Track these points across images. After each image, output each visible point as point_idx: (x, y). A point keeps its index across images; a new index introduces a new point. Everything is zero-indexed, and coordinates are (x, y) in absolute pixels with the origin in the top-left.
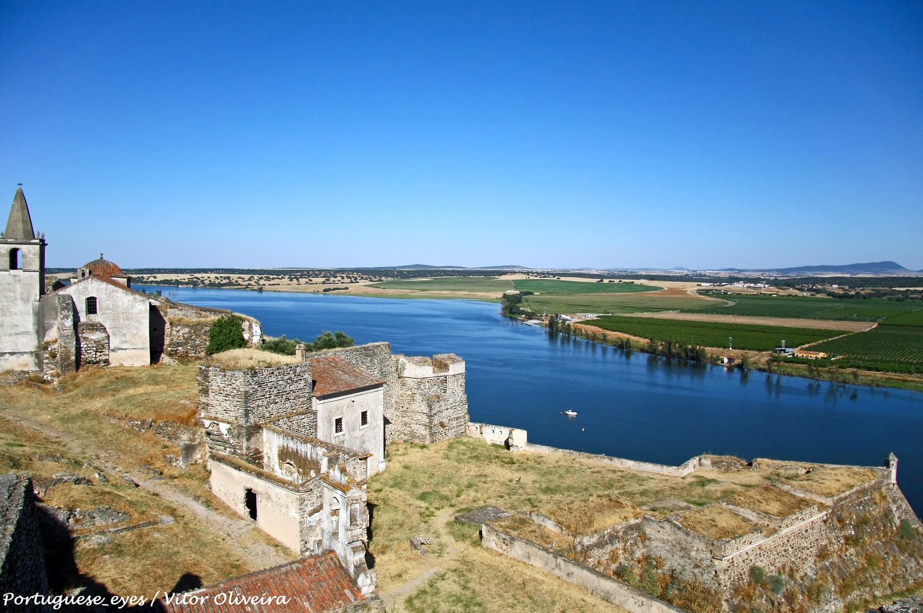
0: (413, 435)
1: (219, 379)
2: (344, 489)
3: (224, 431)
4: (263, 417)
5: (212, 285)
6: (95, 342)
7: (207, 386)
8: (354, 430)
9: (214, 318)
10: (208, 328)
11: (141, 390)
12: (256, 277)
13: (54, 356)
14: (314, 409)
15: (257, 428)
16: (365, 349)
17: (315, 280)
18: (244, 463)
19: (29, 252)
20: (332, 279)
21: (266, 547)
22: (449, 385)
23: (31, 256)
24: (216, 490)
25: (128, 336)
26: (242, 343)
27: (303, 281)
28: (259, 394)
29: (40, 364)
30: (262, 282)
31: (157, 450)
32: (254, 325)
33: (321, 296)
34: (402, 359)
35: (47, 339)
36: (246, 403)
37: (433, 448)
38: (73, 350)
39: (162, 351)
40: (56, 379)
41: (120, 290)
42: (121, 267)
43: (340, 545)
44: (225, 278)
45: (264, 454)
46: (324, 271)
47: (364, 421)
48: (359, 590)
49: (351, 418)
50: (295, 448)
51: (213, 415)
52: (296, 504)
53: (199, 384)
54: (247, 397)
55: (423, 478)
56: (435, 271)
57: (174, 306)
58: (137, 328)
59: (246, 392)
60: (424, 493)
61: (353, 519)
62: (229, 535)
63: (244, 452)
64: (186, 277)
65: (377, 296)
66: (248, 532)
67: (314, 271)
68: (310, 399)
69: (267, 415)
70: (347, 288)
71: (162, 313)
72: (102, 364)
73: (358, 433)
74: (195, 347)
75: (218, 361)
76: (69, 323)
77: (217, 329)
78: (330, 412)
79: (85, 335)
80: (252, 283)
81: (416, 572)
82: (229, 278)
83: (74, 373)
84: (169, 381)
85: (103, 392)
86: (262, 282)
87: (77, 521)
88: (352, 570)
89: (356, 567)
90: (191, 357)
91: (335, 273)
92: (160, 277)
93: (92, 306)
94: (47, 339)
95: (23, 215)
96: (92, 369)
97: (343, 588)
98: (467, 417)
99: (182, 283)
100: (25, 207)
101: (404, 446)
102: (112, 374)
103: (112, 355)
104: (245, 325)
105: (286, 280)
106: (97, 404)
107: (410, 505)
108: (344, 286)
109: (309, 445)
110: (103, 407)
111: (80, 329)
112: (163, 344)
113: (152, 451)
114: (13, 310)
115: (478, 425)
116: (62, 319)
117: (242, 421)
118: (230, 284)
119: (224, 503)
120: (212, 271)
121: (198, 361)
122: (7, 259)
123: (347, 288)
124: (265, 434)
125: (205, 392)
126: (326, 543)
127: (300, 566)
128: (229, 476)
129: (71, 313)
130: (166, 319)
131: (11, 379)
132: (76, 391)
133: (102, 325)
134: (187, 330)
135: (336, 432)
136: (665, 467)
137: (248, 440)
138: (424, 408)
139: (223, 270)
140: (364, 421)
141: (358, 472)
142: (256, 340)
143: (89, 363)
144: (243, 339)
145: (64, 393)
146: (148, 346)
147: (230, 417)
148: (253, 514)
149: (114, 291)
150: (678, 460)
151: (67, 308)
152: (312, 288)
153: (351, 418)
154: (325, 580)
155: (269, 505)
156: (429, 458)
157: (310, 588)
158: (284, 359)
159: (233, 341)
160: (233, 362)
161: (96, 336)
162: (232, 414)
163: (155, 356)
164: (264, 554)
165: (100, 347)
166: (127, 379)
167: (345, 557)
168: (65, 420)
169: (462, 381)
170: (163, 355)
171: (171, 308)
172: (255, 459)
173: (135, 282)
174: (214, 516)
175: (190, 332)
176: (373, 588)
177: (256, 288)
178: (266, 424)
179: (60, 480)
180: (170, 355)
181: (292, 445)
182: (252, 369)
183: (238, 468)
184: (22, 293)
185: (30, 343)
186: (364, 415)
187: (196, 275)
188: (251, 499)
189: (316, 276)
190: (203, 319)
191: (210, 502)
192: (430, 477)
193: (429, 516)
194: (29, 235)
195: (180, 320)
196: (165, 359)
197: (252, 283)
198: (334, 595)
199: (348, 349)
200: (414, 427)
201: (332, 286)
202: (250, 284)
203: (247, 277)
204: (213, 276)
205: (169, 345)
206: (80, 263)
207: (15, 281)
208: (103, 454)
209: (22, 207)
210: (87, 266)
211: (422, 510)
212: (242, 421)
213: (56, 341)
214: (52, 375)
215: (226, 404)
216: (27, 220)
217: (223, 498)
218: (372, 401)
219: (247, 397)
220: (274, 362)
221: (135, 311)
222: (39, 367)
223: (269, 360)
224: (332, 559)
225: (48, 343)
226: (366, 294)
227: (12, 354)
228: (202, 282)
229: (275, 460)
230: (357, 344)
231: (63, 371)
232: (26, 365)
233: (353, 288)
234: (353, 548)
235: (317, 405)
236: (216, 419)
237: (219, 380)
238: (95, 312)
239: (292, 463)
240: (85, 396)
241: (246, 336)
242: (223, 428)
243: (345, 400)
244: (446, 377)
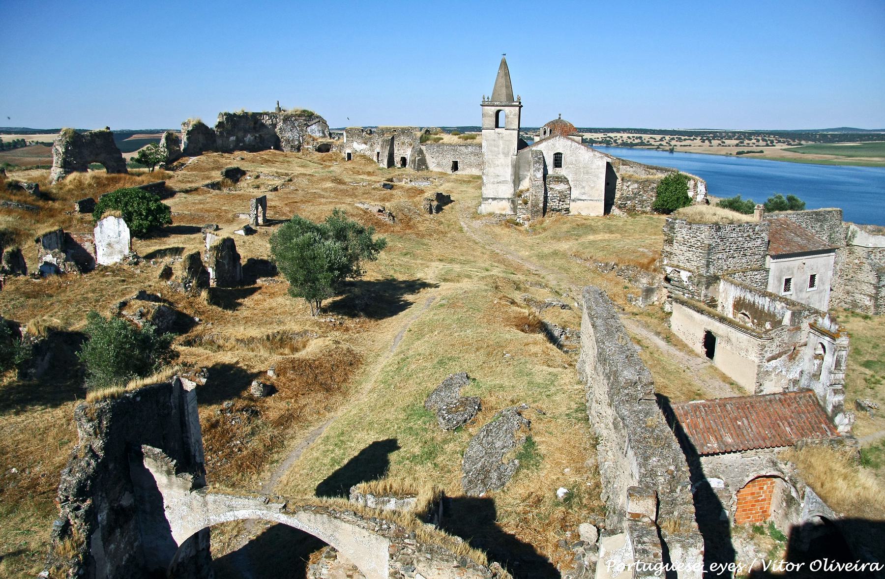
0: (855, 304)
1: (684, 231)
2: (833, 337)
3: (685, 279)
4: (722, 269)
5: (625, 145)
7: (672, 237)
8: (801, 291)
9: (661, 176)
10: (655, 185)
11: (599, 237)
12: (667, 138)
13: (526, 203)
14: (767, 266)
15: (716, 279)
16: (817, 214)
17: (728, 142)
18: (706, 307)
20: (746, 141)
21: (722, 384)
27: (715, 142)
28: (720, 248)
29: (514, 209)
30: (673, 143)
31: (618, 290)
32: (699, 184)
33: (734, 159)
34: (853, 227)
35: (521, 188)
36: (709, 254)
37: (877, 319)
38: (542, 199)
39: (613, 204)
40: (526, 222)
43: (821, 386)
44: (637, 138)
45: (719, 303)
46: (738, 132)
48: (836, 427)
49: (799, 279)
50: (752, 300)
51: (676, 263)
52: (757, 349)
53: (665, 235)
54: (710, 249)
55: (867, 347)
56: (865, 135)
57: (625, 163)
58: (594, 182)
59: (710, 245)
60: (868, 362)
61: (838, 364)
62: (688, 368)
63: (702, 298)
64: (600, 136)
65: (795, 161)
66: (705, 368)
67: (727, 133)
68: (764, 257)
69: (725, 267)
70: (762, 152)
71: (615, 169)
73: (804, 295)
74: (642, 202)
76: (540, 175)
78: (782, 271)
79: (551, 186)
80: (664, 143)
81: (867, 430)
82: (640, 138)
83: (540, 218)
84: (622, 231)
85: (568, 235)
86: (673, 143)
87: (567, 338)
88: (829, 409)
89: (834, 407)
91: (749, 135)
93: (558, 160)
94: (521, 188)
95: (506, 82)
96: (555, 216)
97: (821, 423)
99: (596, 142)
100: (507, 74)
101: (845, 314)
102: (573, 221)
104: (691, 184)
105: (698, 141)
106: (564, 246)
107: (853, 370)
108: (759, 149)
109: (767, 299)
110: (570, 249)
112: (614, 198)
113: (615, 290)
114: (497, 163)
117: (703, 271)
118: (642, 144)
119: (682, 341)
120: (624, 131)
121: (644, 215)
123: (762, 152)
124: (722, 285)
125: (670, 242)
126: (804, 383)
127: (782, 397)
128: (691, 318)
130: (618, 174)
131: (494, 220)
132: (543, 235)
134: (636, 186)
135: (785, 291)
137: (707, 288)
138: (872, 278)
139: (635, 130)
142: (700, 198)
144: (687, 197)
145: (535, 234)
147: (692, 266)
148: (710, 354)
149: (577, 148)
152: (724, 151)
153: (799, 279)
154: (804, 413)
155: (729, 347)
156: (872, 329)
157: (791, 417)
158: (745, 218)
159: (678, 198)
161: (561, 187)
162: (693, 263)
163: (607, 210)
164: (721, 389)
165: (564, 197)
166: (584, 227)
167: (825, 397)
168: (541, 257)
170: (614, 207)
171: (623, 165)
174: (673, 350)
175: (639, 188)
176: (848, 428)
178: (723, 275)
179: (550, 304)
180: (620, 208)
181: (749, 297)
182: (717, 224)
183: (701, 311)
184: (504, 148)
185: (507, 191)
186: (813, 277)
187: (609, 135)
188: (710, 341)
189: (730, 138)
190: (651, 177)
191: (669, 338)
192: (873, 347)
193: (875, 383)
194: (510, 100)
195: (630, 176)
196: (615, 210)
197: (664, 143)
198: (813, 427)
199: (799, 212)
200: (858, 296)
201: (746, 149)
202: (661, 145)
204: (625, 135)
205: (620, 199)
208: (573, 288)
210: (547, 125)
211: (868, 377)
212: (703, 271)
213: (528, 190)
214: (523, 219)
215: (689, 255)
216: (509, 86)
217: (681, 337)
218: (822, 265)
219: (710, 249)
220: (735, 219)
221: (594, 166)
223: (731, 218)
224: (810, 397)
225: (522, 192)
226: (782, 159)
228: (615, 141)
230: (809, 208)
231: (532, 216)
232: (504, 209)
233: (768, 151)
234: (834, 390)
235: (770, 263)
236: (678, 266)
237: (684, 232)
239: (747, 313)
240: (553, 238)
241: (690, 194)
242: (684, 275)
243: (797, 262)
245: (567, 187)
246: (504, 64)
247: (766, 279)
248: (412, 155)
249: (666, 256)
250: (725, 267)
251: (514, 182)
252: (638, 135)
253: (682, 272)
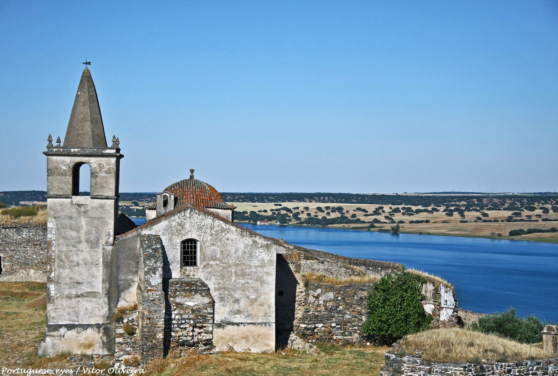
5: (312, 221)
6: (193, 311)
9: (375, 276)
12: (387, 208)
17: (492, 214)
20: (526, 213)
23: (103, 174)
25: (243, 303)
26: (423, 321)
27: (470, 215)
29: (109, 345)
30: (397, 217)
32: (442, 291)
33: (505, 242)
35: (122, 304)
39: (291, 330)
41: (233, 228)
42: (220, 190)
44: (334, 210)
46: (510, 197)
58: (256, 290)
71: (292, 267)
72: (202, 347)
74: (343, 324)
75: (418, 346)
76: (156, 280)
77: (380, 295)
79: (178, 300)
80: (381, 218)
82: (340, 209)
86: (397, 217)
90: (337, 341)
91: (530, 201)
94: (122, 304)
96: (186, 354)
99: (262, 218)
100: (94, 99)
102: (220, 363)
103: (218, 332)
105: (441, 213)
111: (171, 289)
114: (75, 258)
116: (146, 273)
118: (343, 219)
120: (311, 197)
129: (160, 264)
130: (297, 276)
133: (204, 285)
134: (331, 295)
139: (329, 195)
142: (445, 315)
143: (183, 344)
144: (423, 314)
146: (273, 319)
149: (223, 230)
151: (154, 256)
158: (527, 349)
160: (443, 350)
165: (201, 318)
170: (293, 336)
171: (307, 258)
173: (249, 214)
177: (388, 227)
180: (303, 336)
182: (476, 361)
184: (89, 233)
185: (96, 311)
187: (284, 204)
189: (496, 207)
190: (357, 279)
194: (99, 145)
196: (296, 341)
197: (381, 218)
201: (526, 226)
202: (376, 221)
203: (371, 208)
204: (313, 206)
207: (79, 213)
209: (90, 97)
213: (135, 308)
216: (97, 120)
221: (255, 262)
222: (109, 350)
225: (123, 311)
227: (70, 327)
228: (296, 216)
232: (90, 346)
238: (195, 264)
241: (428, 308)
245: (206, 300)
246: (87, 80)
251: (109, 294)
252: (336, 205)
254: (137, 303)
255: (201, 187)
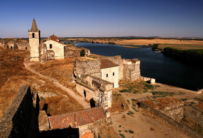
1: (78, 64)
12: (92, 39)
19: (37, 34)
22: (136, 67)
24: (77, 89)
35: (41, 54)
47: (114, 75)
80: (91, 41)
82: (85, 39)
92: (70, 39)
93: (51, 46)
98: (140, 75)
99: (75, 41)
100: (35, 23)
115: (143, 77)
120: (82, 38)
122: (32, 35)
123: (114, 42)
125: (75, 67)
136: (193, 91)
138: (129, 72)
139: (84, 37)
140: (114, 75)
141: (110, 87)
148: (85, 96)
150: (196, 89)
169: (139, 66)
171: (69, 47)
172: (86, 83)
173: (61, 40)
185: (37, 55)
186: (114, 73)
191: (75, 91)
203: (90, 39)
204: (82, 39)
206: (48, 36)
210: (50, 37)
215: (80, 70)
216: (36, 26)
229: (91, 84)
242: (79, 76)
244: (135, 64)
245: (54, 53)
246: (34, 20)
247: (101, 74)
248: (14, 46)
249: (75, 71)
250: (90, 73)
252: (85, 39)
253: (79, 75)
254: (132, 103)
255: (55, 36)
